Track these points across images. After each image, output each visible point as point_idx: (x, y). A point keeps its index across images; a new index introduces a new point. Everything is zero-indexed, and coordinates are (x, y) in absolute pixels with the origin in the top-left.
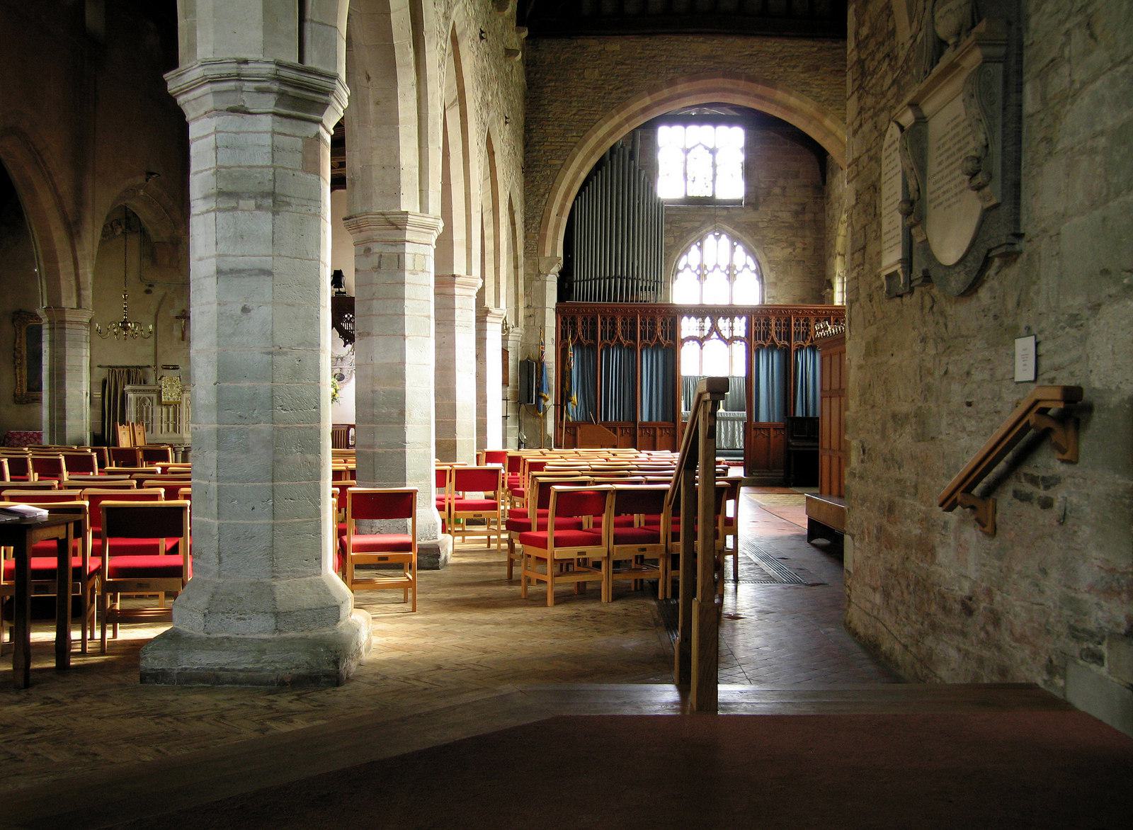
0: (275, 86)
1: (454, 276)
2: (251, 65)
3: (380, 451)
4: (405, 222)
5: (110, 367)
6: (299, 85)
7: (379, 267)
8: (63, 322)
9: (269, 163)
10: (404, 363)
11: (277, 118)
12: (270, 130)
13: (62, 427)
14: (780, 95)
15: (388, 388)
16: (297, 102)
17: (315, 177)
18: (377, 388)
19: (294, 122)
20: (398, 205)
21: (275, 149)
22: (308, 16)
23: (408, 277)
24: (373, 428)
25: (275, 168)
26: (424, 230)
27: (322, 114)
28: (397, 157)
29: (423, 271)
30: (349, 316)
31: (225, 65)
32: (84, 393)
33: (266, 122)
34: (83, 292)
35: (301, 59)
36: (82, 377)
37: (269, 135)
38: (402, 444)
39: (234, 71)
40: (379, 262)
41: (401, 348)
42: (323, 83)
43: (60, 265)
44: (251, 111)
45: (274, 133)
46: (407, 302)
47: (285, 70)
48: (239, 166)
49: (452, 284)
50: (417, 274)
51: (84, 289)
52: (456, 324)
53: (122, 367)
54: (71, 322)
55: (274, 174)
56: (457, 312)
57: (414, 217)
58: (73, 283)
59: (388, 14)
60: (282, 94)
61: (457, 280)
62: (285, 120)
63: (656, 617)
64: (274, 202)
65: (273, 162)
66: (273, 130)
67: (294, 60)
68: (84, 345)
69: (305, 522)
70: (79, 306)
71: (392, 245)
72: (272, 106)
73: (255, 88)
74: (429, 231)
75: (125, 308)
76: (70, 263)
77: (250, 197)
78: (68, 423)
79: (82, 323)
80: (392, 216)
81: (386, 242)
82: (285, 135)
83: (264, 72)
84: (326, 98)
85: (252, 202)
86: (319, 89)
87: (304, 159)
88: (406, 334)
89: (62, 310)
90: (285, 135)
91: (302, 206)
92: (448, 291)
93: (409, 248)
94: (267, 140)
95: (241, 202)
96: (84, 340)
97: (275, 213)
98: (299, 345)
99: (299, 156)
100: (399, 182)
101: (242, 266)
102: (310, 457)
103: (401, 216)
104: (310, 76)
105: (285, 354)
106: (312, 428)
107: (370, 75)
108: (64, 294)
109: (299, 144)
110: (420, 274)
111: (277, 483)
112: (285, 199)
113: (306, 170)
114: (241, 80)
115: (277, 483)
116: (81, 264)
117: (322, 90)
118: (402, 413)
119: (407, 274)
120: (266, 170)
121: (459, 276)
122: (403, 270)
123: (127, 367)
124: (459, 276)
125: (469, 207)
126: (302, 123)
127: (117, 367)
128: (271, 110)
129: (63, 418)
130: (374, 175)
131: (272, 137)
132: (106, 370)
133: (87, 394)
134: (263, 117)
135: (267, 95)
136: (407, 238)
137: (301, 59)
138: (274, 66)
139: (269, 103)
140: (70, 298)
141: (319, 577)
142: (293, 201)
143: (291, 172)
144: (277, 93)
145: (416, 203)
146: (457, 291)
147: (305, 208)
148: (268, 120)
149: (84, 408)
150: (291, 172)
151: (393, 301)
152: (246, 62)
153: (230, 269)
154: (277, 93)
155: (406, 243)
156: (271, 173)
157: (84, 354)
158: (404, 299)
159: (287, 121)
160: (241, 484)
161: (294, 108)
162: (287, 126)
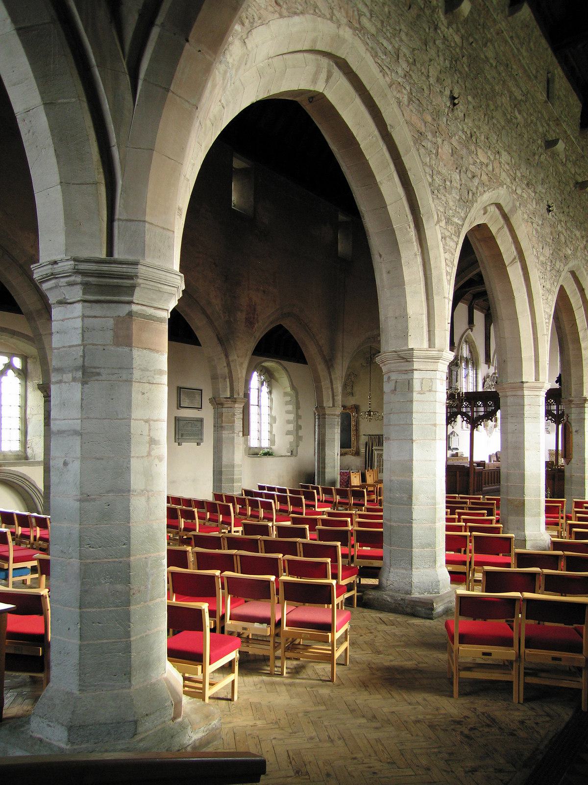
0: (79, 279)
1: (522, 382)
2: (60, 264)
3: (394, 524)
4: (412, 356)
5: (370, 435)
6: (100, 275)
7: (395, 390)
8: (325, 414)
9: (80, 342)
10: (412, 460)
11: (86, 304)
12: (81, 314)
13: (324, 473)
14: (447, 318)
15: (400, 478)
16: (103, 289)
17: (127, 349)
18: (393, 478)
19: (105, 305)
20: (407, 344)
21: (84, 330)
22: (117, 217)
23: (416, 396)
24: (391, 507)
25: (84, 346)
26: (430, 360)
27: (132, 295)
28: (405, 309)
29: (430, 391)
30: (490, 403)
31: (45, 268)
32: (336, 453)
33: (78, 308)
34: (335, 398)
35: (110, 252)
36: (334, 445)
37: (80, 319)
38: (410, 521)
39: (49, 271)
40: (395, 386)
41: (410, 449)
42: (125, 270)
43: (323, 384)
44: (68, 301)
45: (84, 317)
46: (414, 415)
47: (83, 264)
48: (64, 347)
49: (522, 388)
50: (424, 393)
51: (336, 396)
52: (525, 416)
53: (376, 435)
54: (329, 415)
55: (84, 351)
56: (526, 408)
57: (417, 352)
58: (330, 393)
59: (385, 207)
60: (86, 287)
61: (525, 385)
62: (94, 305)
63: (542, 747)
64: (83, 374)
65: (83, 340)
66: (83, 315)
67: (103, 255)
68: (336, 427)
69: (114, 642)
70: (334, 406)
71: (404, 374)
72: (81, 295)
73: (66, 283)
74: (436, 360)
75: (370, 404)
76: (328, 382)
77: (69, 371)
78: (327, 470)
79: (334, 415)
80: (403, 353)
81: (401, 372)
82: (95, 317)
83: (66, 268)
84: (131, 282)
85: (70, 376)
86: (122, 275)
87: (116, 336)
88: (414, 439)
89: (323, 408)
90: (95, 317)
91: (113, 374)
92: (519, 393)
93: (416, 375)
94: (78, 323)
95: (64, 375)
96: (336, 424)
97: (84, 383)
98: (108, 492)
99: (111, 333)
100: (407, 327)
101: (64, 428)
102: (119, 587)
103: (409, 352)
104: (112, 266)
105: (94, 500)
106: (121, 562)
107: (381, 254)
108: (325, 400)
109: (111, 322)
110: (427, 393)
111: (84, 610)
112: (94, 370)
113: (117, 344)
114: (57, 278)
115: (84, 610)
116: (334, 382)
117: (125, 275)
118: (410, 497)
119: (415, 394)
120: (78, 348)
121: (527, 382)
122: (412, 391)
123: (378, 435)
124: (527, 382)
125: (535, 332)
126: (113, 305)
127: (373, 435)
128: (79, 299)
129: (324, 468)
130: (389, 324)
131: (83, 321)
132: (367, 437)
133: (338, 454)
134: (76, 305)
135: (75, 287)
136: (415, 367)
137: (110, 252)
138: (72, 262)
139: (77, 293)
140: (328, 401)
141: (127, 691)
142: (102, 371)
143: (101, 348)
144: (81, 284)
145: (423, 340)
146: (526, 393)
147: (116, 376)
148: (79, 307)
149: (336, 462)
150: (101, 348)
151: (405, 414)
152: (55, 263)
153: (58, 431)
154: (81, 284)
155: (415, 372)
156: (82, 350)
157: (336, 432)
158: (412, 413)
159: (97, 306)
160: (63, 607)
161: (102, 294)
162: (97, 310)
